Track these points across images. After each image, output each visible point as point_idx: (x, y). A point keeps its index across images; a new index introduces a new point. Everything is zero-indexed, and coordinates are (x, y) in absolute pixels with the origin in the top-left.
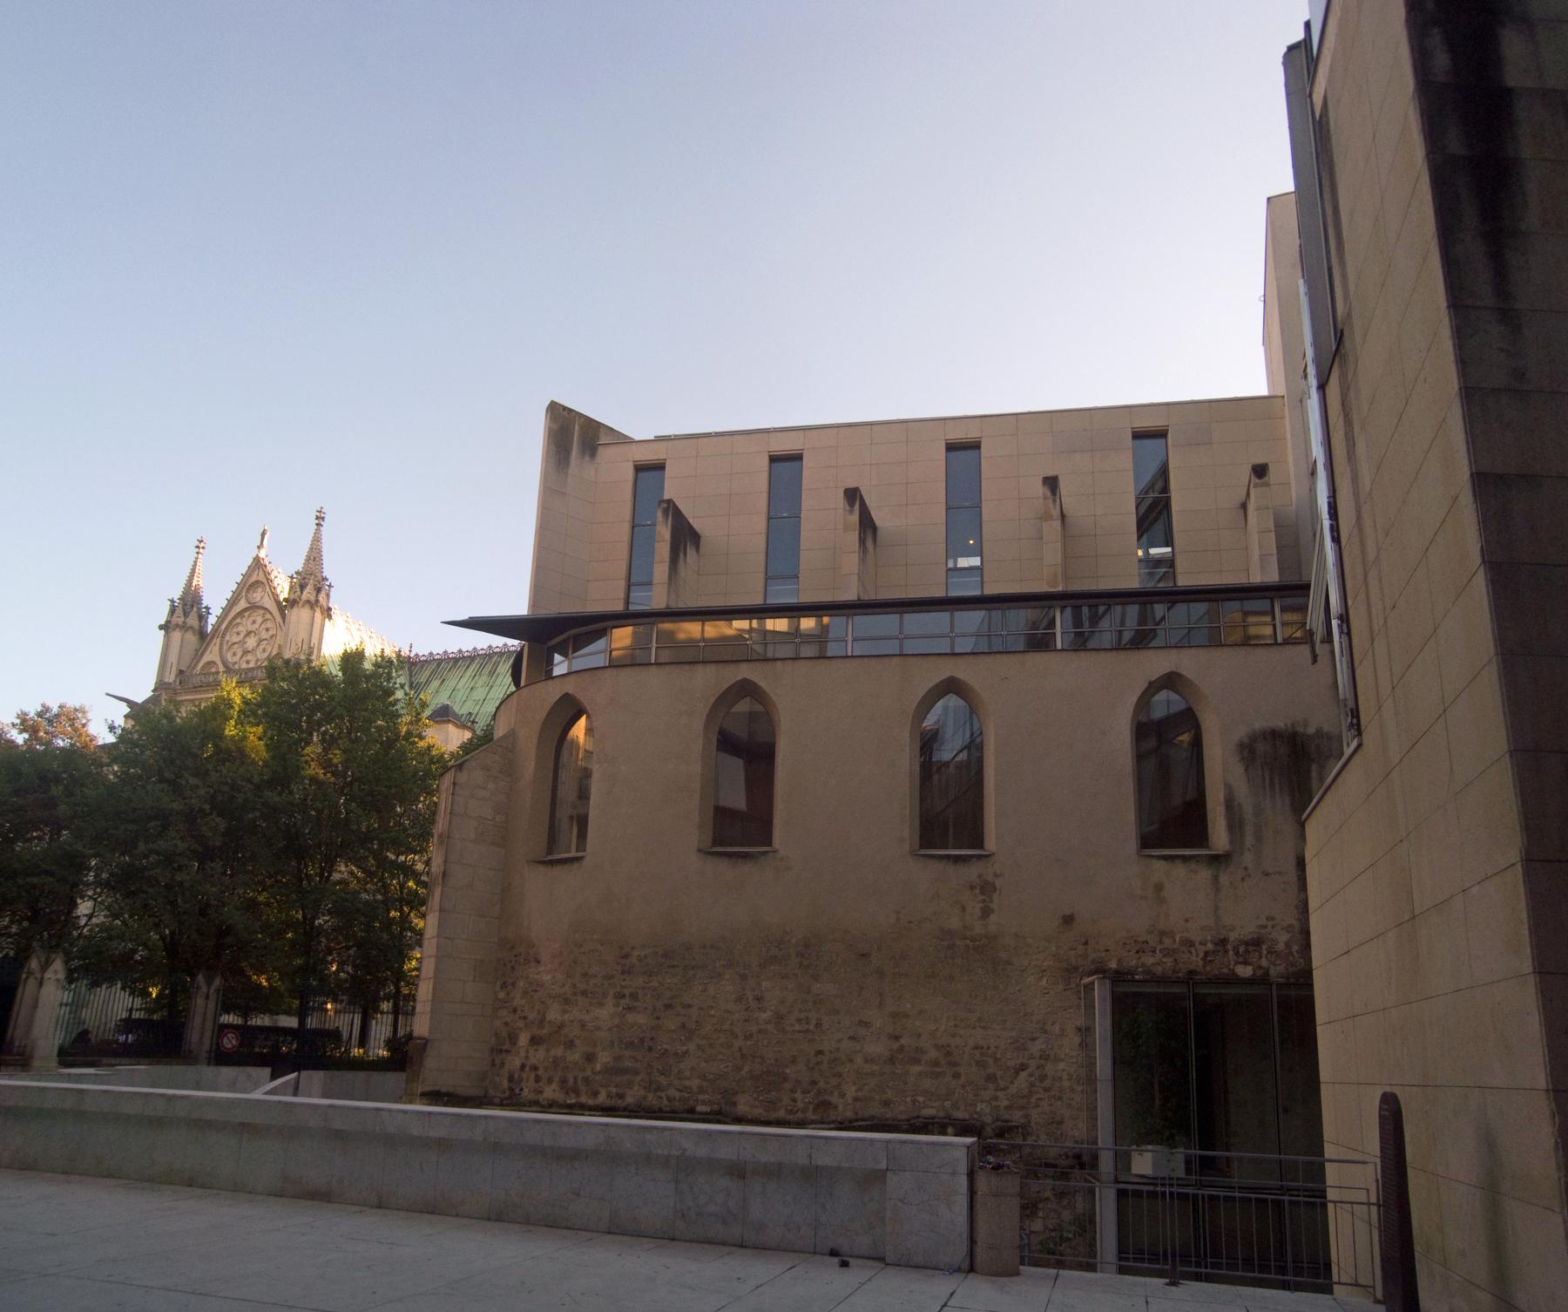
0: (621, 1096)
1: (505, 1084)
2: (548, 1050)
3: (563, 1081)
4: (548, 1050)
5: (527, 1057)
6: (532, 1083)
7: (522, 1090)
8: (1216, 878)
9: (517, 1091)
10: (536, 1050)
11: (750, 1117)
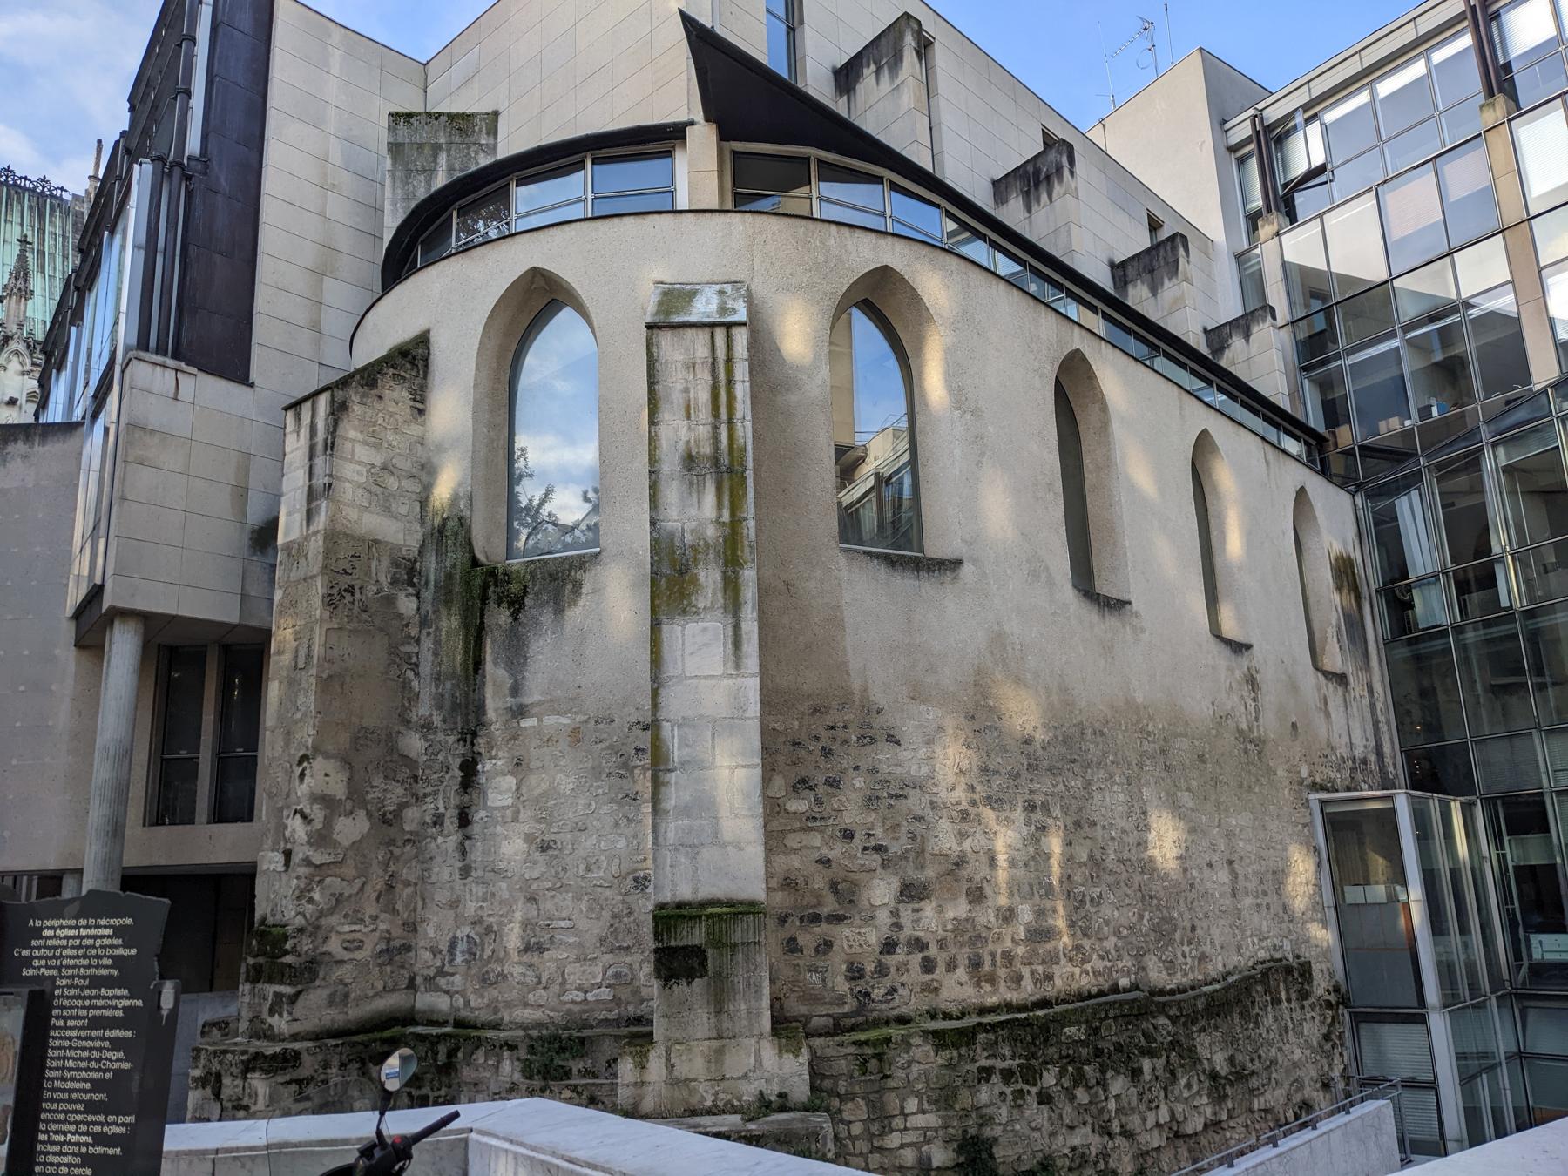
0: (1049, 977)
1: (842, 986)
2: (940, 910)
3: (975, 964)
4: (940, 910)
5: (898, 926)
6: (916, 976)
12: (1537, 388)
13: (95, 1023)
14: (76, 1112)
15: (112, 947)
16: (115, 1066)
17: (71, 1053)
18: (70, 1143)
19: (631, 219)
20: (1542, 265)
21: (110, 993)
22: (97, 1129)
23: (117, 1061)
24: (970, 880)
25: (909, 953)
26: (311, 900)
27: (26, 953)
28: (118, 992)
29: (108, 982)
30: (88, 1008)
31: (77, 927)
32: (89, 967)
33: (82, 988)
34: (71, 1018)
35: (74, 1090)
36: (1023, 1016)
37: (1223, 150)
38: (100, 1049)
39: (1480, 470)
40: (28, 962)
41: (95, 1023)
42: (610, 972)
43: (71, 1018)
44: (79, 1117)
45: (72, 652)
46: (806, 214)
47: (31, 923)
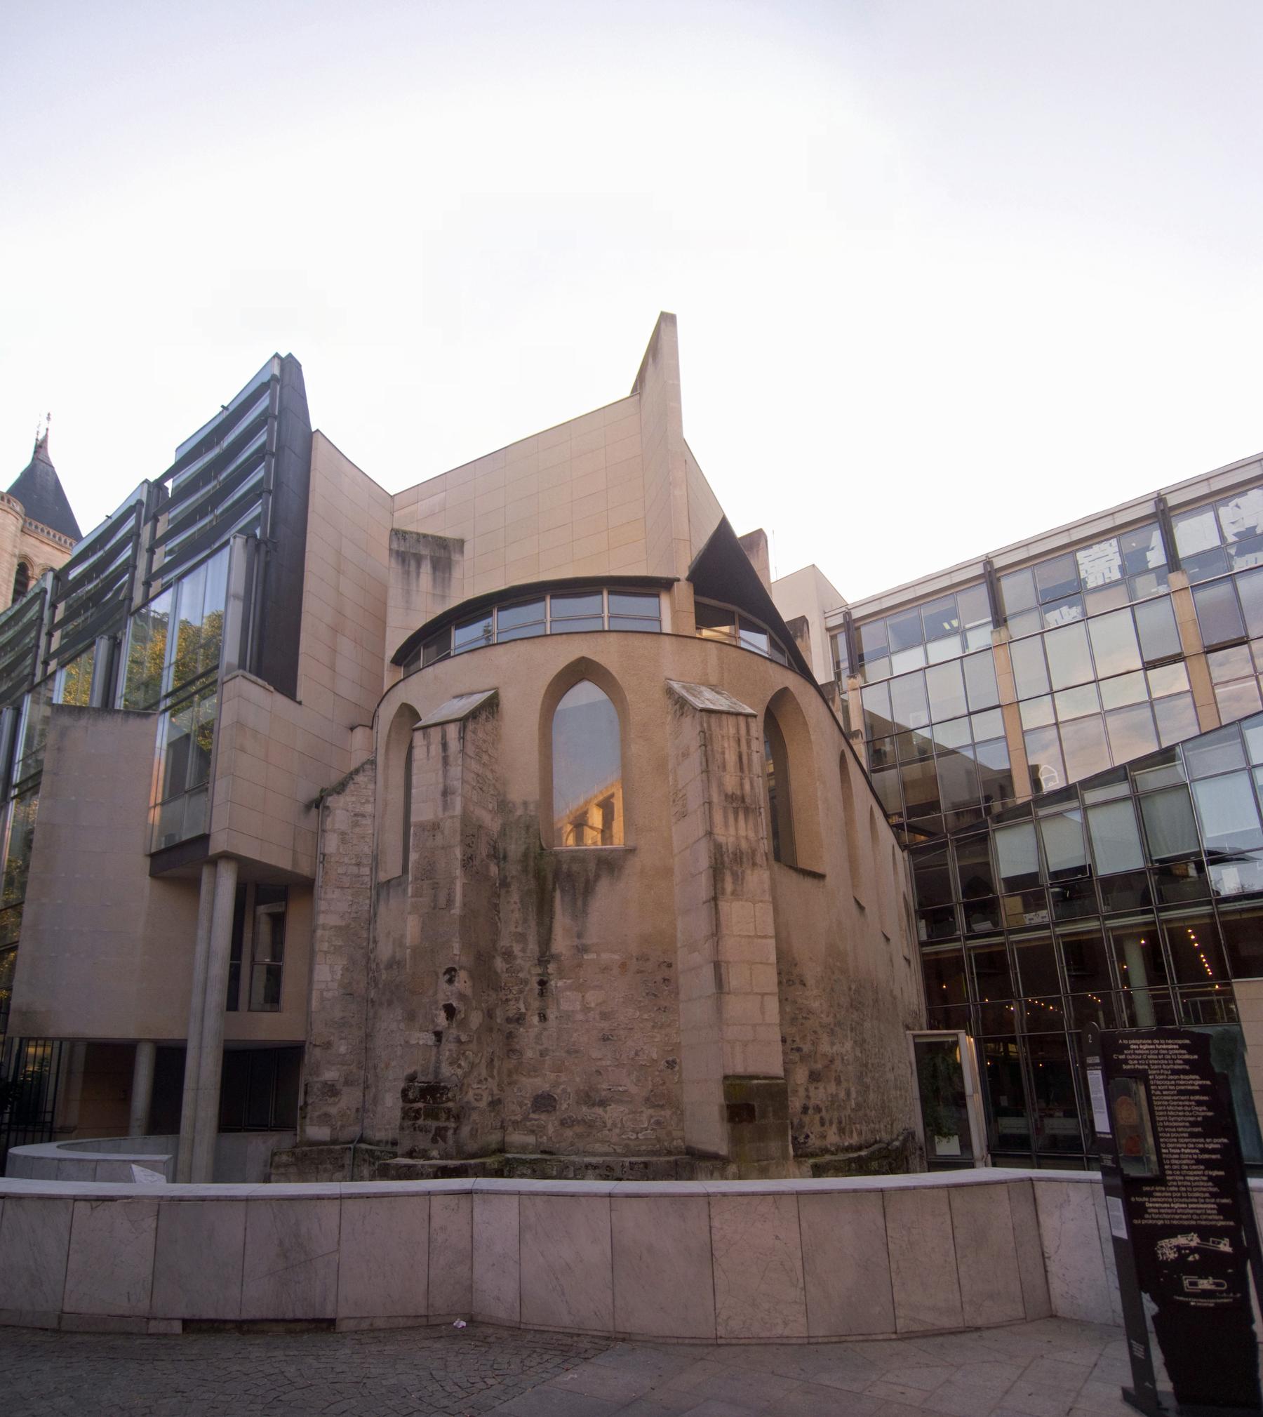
5: (808, 1097)
6: (817, 1128)
7: (807, 1137)
8: (323, 912)
9: (801, 1139)
10: (816, 1088)
11: (305, 1337)
12: (1019, 801)
13: (1181, 1093)
14: (1184, 1138)
15: (1180, 1054)
16: (1203, 1114)
17: (1170, 1108)
18: (1184, 1153)
19: (615, 634)
20: (1025, 728)
21: (1187, 1077)
22: (1201, 1146)
23: (1203, 1112)
24: (836, 1071)
25: (814, 1114)
26: (460, 1066)
27: (1121, 1057)
28: (1193, 1077)
29: (1184, 1072)
30: (1175, 1085)
31: (1153, 1044)
32: (1168, 1064)
33: (1167, 1075)
34: (1165, 1090)
35: (1179, 1127)
36: (855, 1155)
37: (824, 631)
38: (1190, 1106)
39: (987, 844)
40: (1126, 1062)
41: (1181, 1093)
42: (652, 1121)
43: (1165, 1090)
44: (1186, 1140)
45: (148, 880)
46: (601, 629)
47: (1120, 1041)
